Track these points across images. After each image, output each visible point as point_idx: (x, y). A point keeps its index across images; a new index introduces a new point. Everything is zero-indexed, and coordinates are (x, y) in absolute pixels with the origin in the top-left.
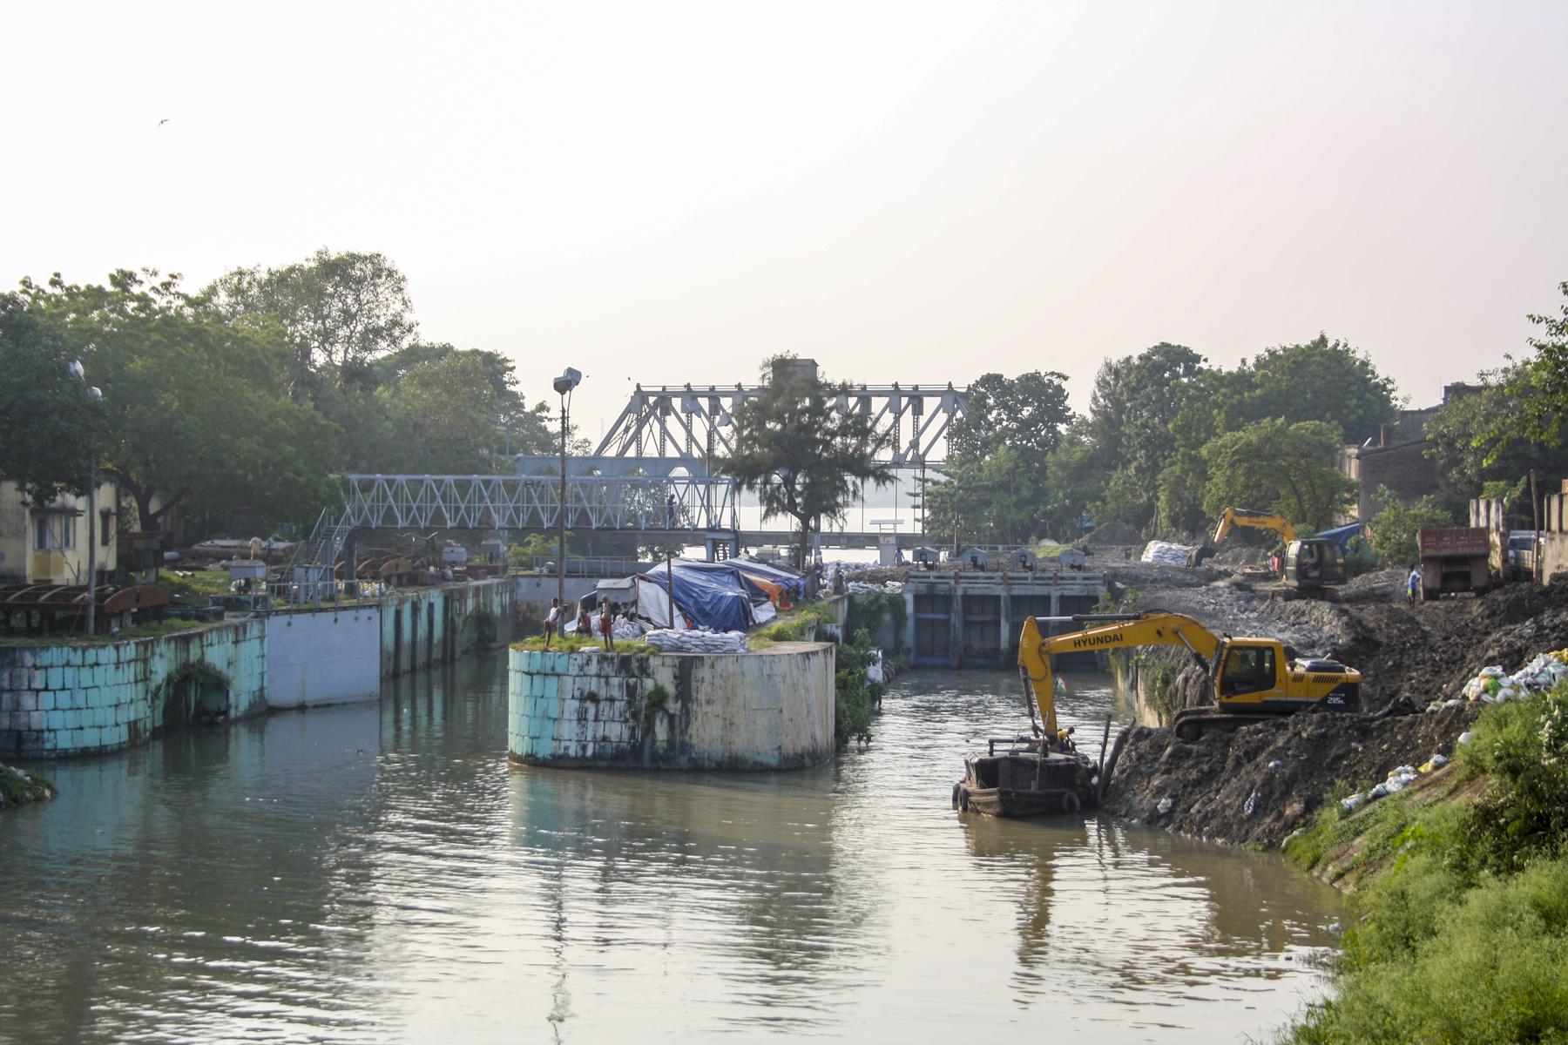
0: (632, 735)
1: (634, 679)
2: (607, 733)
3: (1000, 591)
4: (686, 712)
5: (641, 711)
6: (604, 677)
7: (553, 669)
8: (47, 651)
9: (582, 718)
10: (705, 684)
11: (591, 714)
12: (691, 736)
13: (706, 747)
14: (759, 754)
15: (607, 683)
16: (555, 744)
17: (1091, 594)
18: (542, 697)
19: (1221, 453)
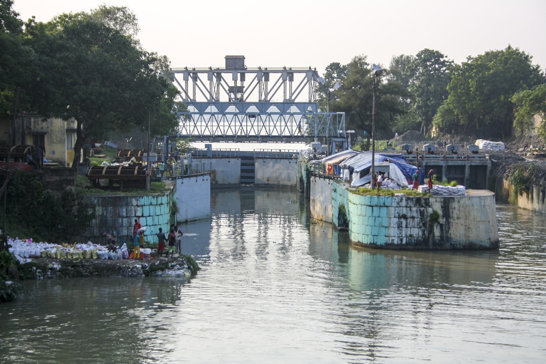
0: (424, 234)
1: (423, 208)
2: (412, 233)
3: (442, 163)
4: (448, 223)
5: (427, 222)
6: (409, 207)
7: (384, 204)
8: (142, 198)
9: (399, 226)
10: (456, 210)
11: (404, 224)
12: (451, 234)
13: (458, 239)
14: (482, 241)
15: (411, 210)
16: (386, 238)
17: (484, 164)
18: (379, 217)
19: (523, 100)
